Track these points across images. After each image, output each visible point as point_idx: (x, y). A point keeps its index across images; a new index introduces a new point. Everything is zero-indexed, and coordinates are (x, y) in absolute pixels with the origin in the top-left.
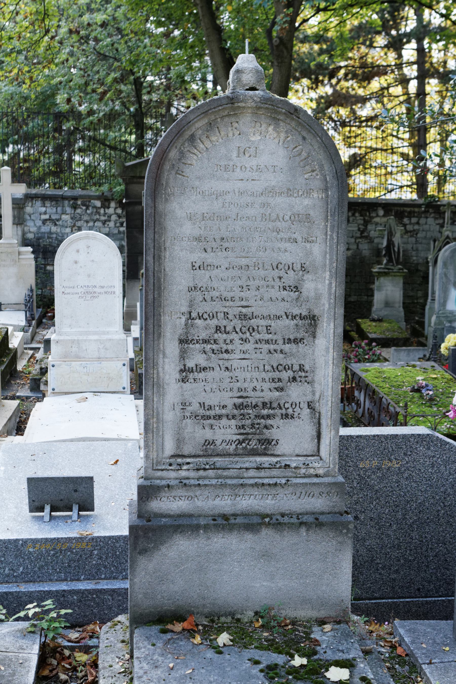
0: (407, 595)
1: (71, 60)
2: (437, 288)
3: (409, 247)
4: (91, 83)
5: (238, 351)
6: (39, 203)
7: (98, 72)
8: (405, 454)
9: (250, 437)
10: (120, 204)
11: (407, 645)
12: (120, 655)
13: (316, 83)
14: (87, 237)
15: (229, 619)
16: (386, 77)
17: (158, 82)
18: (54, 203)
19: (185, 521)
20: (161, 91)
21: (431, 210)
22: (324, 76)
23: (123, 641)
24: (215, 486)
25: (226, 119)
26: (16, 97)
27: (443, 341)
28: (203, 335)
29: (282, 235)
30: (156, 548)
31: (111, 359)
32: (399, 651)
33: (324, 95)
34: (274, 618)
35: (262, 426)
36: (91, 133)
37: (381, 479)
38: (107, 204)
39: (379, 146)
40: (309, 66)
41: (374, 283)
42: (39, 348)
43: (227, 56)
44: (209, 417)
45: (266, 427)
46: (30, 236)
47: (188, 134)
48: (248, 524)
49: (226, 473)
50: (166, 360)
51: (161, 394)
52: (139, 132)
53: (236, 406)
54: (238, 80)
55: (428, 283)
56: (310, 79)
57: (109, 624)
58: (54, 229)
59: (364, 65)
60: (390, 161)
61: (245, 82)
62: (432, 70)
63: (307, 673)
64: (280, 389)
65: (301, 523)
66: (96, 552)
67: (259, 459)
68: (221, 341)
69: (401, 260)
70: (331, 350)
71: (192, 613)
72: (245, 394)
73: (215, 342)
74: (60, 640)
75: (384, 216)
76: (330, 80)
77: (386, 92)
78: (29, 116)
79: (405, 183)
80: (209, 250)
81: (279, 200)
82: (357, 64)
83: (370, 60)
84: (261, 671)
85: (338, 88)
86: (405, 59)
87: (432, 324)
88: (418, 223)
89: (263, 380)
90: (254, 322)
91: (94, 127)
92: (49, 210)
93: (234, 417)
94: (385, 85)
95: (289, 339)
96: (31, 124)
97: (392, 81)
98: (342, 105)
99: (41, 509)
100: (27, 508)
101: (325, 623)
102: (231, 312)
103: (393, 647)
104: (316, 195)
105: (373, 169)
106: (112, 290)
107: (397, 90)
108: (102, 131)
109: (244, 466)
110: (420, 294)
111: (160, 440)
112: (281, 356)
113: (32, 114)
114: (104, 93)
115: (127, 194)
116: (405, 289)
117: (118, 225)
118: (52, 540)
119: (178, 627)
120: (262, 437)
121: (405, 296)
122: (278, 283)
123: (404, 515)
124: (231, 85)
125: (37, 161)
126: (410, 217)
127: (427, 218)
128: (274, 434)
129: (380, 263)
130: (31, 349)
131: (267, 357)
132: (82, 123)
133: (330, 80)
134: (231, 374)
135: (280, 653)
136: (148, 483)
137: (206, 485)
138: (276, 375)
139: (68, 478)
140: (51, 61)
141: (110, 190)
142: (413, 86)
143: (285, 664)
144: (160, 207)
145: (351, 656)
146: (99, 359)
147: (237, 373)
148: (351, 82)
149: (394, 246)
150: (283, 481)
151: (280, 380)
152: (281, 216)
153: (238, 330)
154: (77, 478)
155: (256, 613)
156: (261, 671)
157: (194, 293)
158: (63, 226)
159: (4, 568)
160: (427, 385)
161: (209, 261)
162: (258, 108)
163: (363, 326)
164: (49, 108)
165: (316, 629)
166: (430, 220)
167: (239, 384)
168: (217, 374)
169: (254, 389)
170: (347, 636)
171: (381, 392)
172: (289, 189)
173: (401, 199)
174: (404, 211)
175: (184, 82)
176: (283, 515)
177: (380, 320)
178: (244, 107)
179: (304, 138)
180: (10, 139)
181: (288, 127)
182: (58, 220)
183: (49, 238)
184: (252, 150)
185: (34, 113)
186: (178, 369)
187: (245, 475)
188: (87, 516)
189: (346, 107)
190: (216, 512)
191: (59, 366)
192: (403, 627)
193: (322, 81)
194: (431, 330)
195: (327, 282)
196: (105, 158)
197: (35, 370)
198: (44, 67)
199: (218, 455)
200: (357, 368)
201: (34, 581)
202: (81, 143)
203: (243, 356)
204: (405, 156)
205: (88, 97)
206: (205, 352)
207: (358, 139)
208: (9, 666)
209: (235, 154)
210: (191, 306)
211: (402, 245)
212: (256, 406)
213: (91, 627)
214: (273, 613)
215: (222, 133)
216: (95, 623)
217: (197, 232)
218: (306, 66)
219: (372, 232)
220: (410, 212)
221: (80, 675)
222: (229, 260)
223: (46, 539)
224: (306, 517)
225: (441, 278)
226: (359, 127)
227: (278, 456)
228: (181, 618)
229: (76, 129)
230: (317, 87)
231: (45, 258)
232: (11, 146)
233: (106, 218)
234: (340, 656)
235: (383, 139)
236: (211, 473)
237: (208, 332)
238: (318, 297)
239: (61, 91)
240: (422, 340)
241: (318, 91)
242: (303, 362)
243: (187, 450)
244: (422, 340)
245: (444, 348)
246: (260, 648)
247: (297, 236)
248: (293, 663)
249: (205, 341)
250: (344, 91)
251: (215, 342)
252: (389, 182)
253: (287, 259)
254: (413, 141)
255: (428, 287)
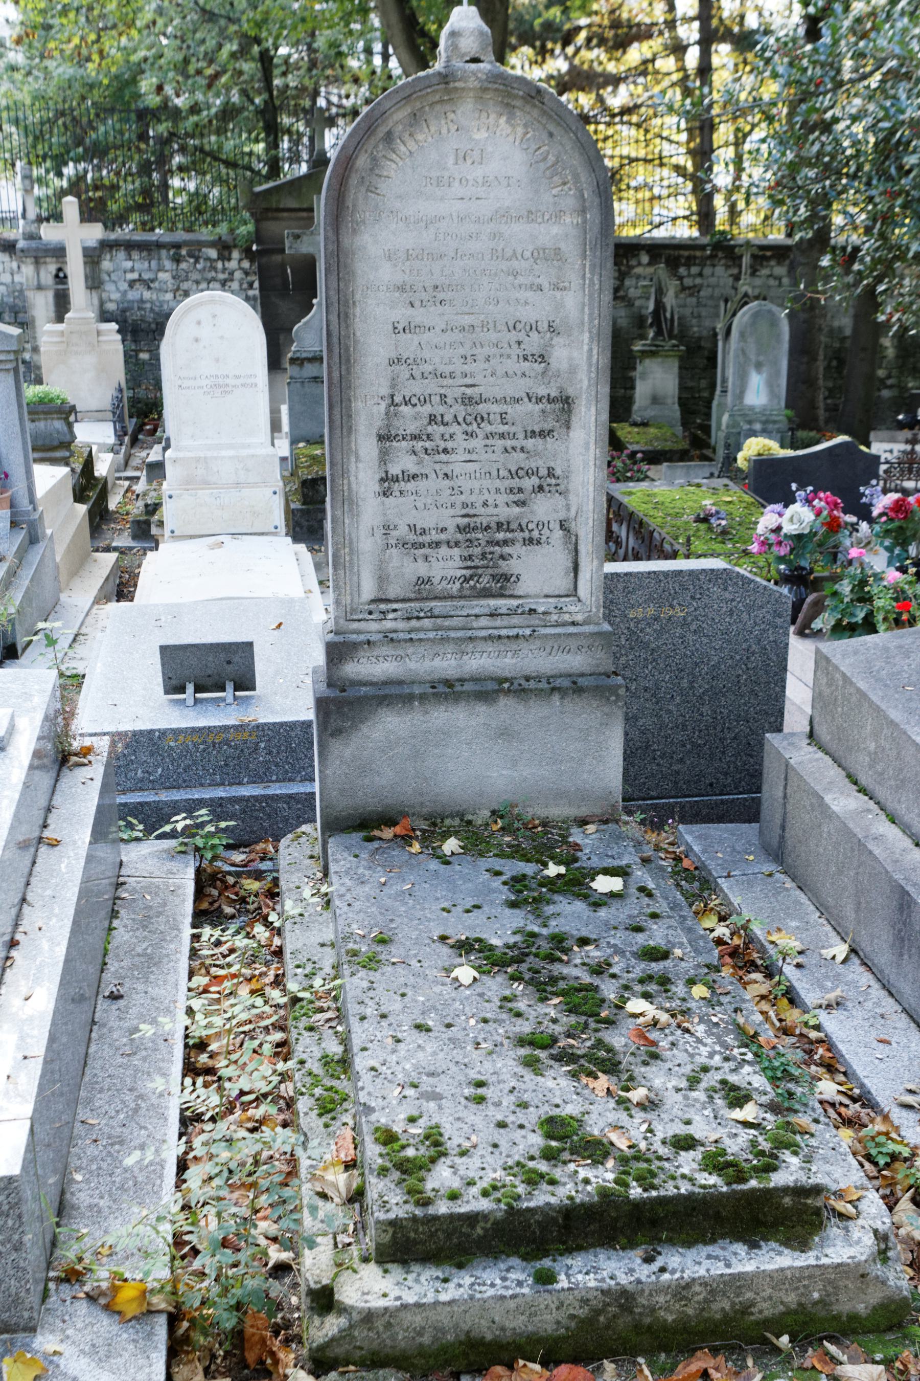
0: (696, 792)
1: (160, 22)
2: (730, 373)
3: (687, 312)
4: (194, 60)
5: (460, 451)
6: (121, 254)
7: (203, 41)
8: (693, 598)
9: (480, 571)
10: (248, 253)
11: (696, 855)
12: (309, 873)
13: (543, 53)
14: (212, 301)
15: (457, 821)
16: (651, 42)
17: (296, 56)
18: (144, 254)
19: (394, 690)
20: (302, 72)
21: (720, 254)
22: (555, 42)
23: (312, 857)
24: (432, 641)
25: (438, 107)
26: (77, 85)
27: (739, 449)
28: (412, 428)
29: (521, 280)
30: (355, 727)
31: (255, 485)
32: (686, 863)
33: (555, 73)
34: (518, 818)
35: (496, 556)
36: (197, 142)
37: (659, 633)
38: (226, 253)
39: (642, 154)
40: (532, 26)
41: (634, 369)
42: (138, 478)
43: (408, 11)
44: (422, 545)
45: (502, 557)
46: (111, 307)
47: (381, 131)
48: (481, 692)
49: (447, 623)
50: (360, 465)
51: (355, 515)
52: (271, 138)
53: (460, 529)
54: (454, 48)
55: (715, 366)
56: (534, 47)
57: (290, 836)
58: (147, 295)
59: (616, 24)
60: (657, 178)
61: (463, 50)
62: (722, 29)
63: (566, 884)
64: (522, 503)
65: (553, 689)
66: (263, 745)
67: (493, 602)
68: (437, 437)
69: (676, 331)
70: (592, 446)
71: (405, 815)
72: (472, 512)
73: (429, 437)
74: (219, 864)
75: (650, 264)
76: (563, 48)
77: (650, 66)
78: (97, 115)
79: (682, 213)
80: (417, 304)
81: (517, 228)
82: (606, 22)
83: (625, 16)
84: (505, 883)
85: (577, 61)
86: (679, 13)
87: (724, 427)
88: (700, 275)
89: (498, 491)
90: (482, 408)
91: (199, 131)
92: (138, 266)
93: (457, 544)
94: (649, 56)
95: (533, 432)
96: (102, 129)
97: (661, 48)
98: (583, 90)
99: (181, 689)
100: (161, 689)
101: (587, 823)
102: (451, 394)
103: (678, 859)
104: (568, 220)
105: (632, 192)
106: (252, 380)
107: (667, 64)
108: (213, 138)
109: (473, 612)
110: (704, 383)
111: (355, 578)
112: (522, 455)
113: (103, 112)
114: (216, 76)
115: (258, 237)
116: (681, 378)
117: (245, 286)
118: (200, 730)
119: (388, 833)
120: (496, 571)
121: (682, 388)
122: (515, 351)
123: (691, 682)
124: (443, 55)
125: (115, 188)
126: (688, 266)
127: (714, 266)
128: (513, 566)
129: (643, 337)
130: (127, 478)
131: (502, 458)
132: (181, 125)
133: (563, 48)
134: (452, 483)
135: (528, 861)
136: (340, 639)
137: (420, 640)
138: (516, 483)
139: (218, 645)
140: (131, 24)
141: (232, 231)
142: (692, 57)
143: (536, 874)
144: (346, 241)
145: (624, 863)
146: (238, 485)
147: (460, 482)
148: (596, 51)
149: (665, 311)
150: (528, 632)
151: (520, 490)
152: (519, 251)
153: (460, 419)
154: (230, 644)
155: (493, 813)
156: (505, 883)
157: (396, 368)
158: (160, 290)
159: (136, 770)
160: (717, 512)
161: (418, 320)
162: (485, 90)
163: (619, 433)
164: (129, 103)
165: (575, 830)
166: (720, 270)
167: (463, 498)
168: (432, 483)
169: (485, 504)
170: (619, 837)
171: (653, 523)
172: (530, 212)
173: (674, 238)
174: (680, 256)
175: (340, 54)
176: (527, 679)
177: (645, 424)
178: (463, 89)
179: (551, 135)
180: (72, 154)
181: (528, 117)
182: (152, 281)
183: (139, 309)
184: (476, 153)
185: (105, 110)
186: (378, 477)
187: (475, 625)
188: (247, 697)
189: (590, 92)
190: (436, 676)
191: (179, 496)
192: (690, 833)
193: (552, 51)
194: (722, 435)
195: (586, 348)
196: (219, 180)
197: (136, 509)
198: (120, 34)
199: (436, 598)
200: (619, 490)
201: (178, 787)
202: (177, 159)
203: (468, 457)
204: (679, 170)
205: (190, 82)
206: (414, 453)
207: (609, 143)
208: (157, 894)
209: (451, 161)
210: (393, 386)
211: (676, 310)
212: (488, 527)
213: (262, 845)
214: (516, 811)
215: (433, 129)
216: (267, 841)
217: (399, 278)
218: (527, 26)
219: (632, 290)
220: (689, 258)
221: (251, 907)
222: (446, 318)
223: (193, 729)
224: (559, 681)
225: (736, 356)
226: (608, 124)
227: (520, 597)
228: (391, 822)
229: (172, 135)
230: (544, 61)
231: (135, 341)
232: (71, 164)
233: (226, 276)
234: (609, 863)
235: (647, 142)
236: (427, 623)
237: (418, 424)
238: (573, 370)
239: (148, 74)
240: (708, 452)
241: (545, 66)
242: (552, 464)
243: (393, 591)
244: (708, 452)
245: (742, 459)
246: (501, 855)
247: (544, 281)
248: (546, 872)
249: (415, 437)
250: (586, 67)
251: (429, 437)
252: (656, 211)
253: (528, 314)
254: (692, 145)
255: (715, 374)
